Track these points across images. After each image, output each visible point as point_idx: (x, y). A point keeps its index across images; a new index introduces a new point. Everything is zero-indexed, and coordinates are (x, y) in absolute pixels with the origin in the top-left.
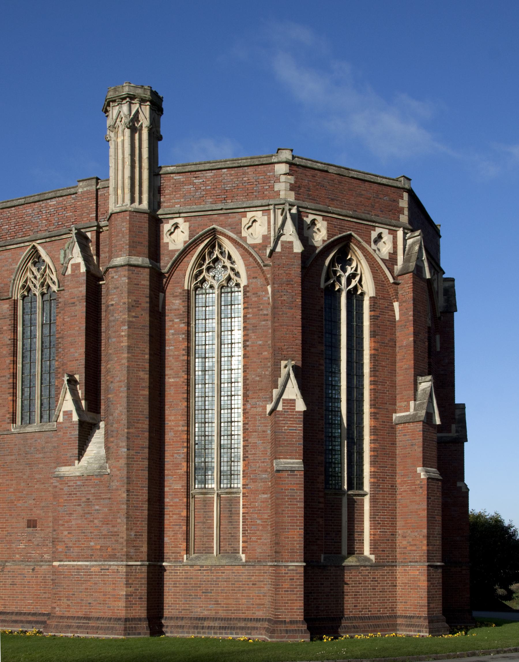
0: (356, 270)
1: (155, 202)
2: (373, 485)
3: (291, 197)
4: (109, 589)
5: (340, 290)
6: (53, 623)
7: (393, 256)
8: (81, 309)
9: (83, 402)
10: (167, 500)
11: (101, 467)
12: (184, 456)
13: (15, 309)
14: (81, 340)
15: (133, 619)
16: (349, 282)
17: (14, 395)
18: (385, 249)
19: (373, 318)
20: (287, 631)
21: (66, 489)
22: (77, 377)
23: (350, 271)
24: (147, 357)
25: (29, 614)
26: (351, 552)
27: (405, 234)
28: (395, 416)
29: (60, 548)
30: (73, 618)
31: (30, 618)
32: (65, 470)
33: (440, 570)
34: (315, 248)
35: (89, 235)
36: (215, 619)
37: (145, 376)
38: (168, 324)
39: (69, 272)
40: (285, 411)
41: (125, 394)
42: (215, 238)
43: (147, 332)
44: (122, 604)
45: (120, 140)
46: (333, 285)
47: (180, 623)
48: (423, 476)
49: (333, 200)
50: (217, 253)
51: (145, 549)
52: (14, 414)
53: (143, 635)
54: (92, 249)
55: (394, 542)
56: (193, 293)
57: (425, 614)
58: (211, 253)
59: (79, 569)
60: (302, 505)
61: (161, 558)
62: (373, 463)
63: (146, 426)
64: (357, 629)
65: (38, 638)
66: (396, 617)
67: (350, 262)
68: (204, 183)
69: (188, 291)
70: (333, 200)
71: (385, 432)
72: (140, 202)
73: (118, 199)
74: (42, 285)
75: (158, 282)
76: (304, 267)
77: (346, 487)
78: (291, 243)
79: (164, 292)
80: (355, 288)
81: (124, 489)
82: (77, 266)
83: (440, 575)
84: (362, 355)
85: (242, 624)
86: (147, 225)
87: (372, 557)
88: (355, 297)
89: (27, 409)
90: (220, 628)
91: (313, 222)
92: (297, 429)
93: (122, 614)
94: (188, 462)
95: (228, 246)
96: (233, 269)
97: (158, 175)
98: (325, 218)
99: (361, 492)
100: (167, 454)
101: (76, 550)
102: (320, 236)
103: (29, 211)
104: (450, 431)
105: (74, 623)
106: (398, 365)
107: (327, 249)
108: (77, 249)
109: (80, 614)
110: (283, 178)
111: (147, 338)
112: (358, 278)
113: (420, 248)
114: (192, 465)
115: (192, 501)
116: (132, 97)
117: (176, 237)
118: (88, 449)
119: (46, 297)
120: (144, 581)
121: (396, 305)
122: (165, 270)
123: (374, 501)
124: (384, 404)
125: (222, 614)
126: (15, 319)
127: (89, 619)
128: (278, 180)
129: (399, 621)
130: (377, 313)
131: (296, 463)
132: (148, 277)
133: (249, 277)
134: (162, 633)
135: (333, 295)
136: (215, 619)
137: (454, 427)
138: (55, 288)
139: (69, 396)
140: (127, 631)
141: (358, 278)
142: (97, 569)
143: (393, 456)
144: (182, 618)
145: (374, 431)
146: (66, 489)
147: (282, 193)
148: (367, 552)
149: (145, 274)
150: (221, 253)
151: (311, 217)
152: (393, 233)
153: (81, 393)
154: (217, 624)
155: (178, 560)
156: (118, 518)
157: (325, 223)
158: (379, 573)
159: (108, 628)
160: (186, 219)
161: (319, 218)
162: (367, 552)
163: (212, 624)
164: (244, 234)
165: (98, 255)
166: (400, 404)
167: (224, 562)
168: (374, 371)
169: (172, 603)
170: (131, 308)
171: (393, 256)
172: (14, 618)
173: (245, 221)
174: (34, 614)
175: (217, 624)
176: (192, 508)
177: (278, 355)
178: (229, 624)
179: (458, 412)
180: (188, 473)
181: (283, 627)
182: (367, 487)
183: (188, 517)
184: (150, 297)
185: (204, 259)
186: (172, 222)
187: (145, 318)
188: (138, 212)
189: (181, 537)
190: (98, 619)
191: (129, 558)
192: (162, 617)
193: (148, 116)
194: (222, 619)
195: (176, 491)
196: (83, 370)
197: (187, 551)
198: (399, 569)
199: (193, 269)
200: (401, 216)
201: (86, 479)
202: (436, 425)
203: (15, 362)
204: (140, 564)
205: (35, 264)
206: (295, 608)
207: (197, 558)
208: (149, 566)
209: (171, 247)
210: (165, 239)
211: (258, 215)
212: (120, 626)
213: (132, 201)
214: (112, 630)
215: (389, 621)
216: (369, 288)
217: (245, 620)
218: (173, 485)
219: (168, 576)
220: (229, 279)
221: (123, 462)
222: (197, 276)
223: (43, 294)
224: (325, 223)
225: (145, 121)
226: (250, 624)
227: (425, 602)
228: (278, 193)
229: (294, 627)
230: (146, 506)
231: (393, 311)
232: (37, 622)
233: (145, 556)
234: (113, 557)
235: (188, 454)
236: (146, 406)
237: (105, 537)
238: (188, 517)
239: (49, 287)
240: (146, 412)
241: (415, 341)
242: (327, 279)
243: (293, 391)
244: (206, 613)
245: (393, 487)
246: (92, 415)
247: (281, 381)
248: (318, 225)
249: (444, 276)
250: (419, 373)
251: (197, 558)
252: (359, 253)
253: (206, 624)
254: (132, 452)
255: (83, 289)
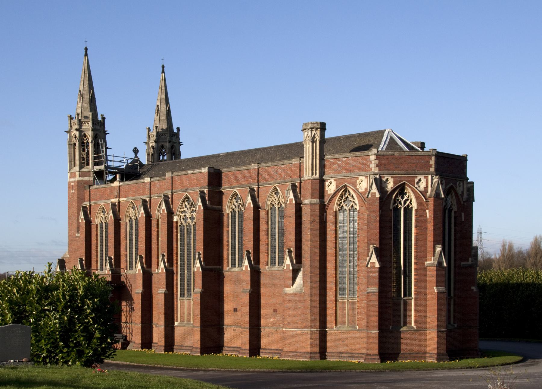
0: (409, 197)
1: (322, 173)
2: (415, 294)
3: (377, 170)
4: (304, 340)
5: (400, 208)
6: (283, 354)
7: (426, 189)
8: (293, 219)
9: (294, 260)
10: (327, 303)
11: (301, 289)
12: (334, 284)
13: (268, 214)
14: (293, 233)
15: (314, 353)
16: (405, 203)
17: (268, 253)
18: (422, 185)
19: (416, 219)
20: (371, 359)
21: (287, 298)
22: (292, 249)
23: (405, 198)
24: (318, 243)
25: (275, 350)
26: (405, 324)
27: (432, 177)
28: (426, 263)
29: (286, 323)
30: (291, 352)
31: (276, 351)
32: (287, 290)
33: (445, 333)
34: (387, 191)
35: (297, 184)
36: (347, 353)
37: (317, 251)
38: (328, 226)
39: (288, 202)
40: (371, 267)
41: (309, 259)
42: (346, 188)
43: (318, 232)
44: (309, 346)
45: (308, 146)
46: (397, 206)
47: (333, 355)
48: (436, 291)
49: (396, 168)
50: (347, 194)
51: (318, 324)
52: (267, 262)
53: (318, 360)
54: (298, 190)
55: (425, 320)
56: (338, 212)
57: (436, 352)
58: (345, 194)
59: (293, 332)
60: (377, 307)
61: (325, 327)
62: (415, 285)
63: (318, 272)
64: (406, 358)
65: (278, 361)
66: (426, 353)
67: (406, 194)
68: (342, 164)
69: (336, 212)
70: (396, 168)
71: (422, 270)
72: (316, 174)
73: (307, 175)
74: (279, 203)
75: (323, 208)
76: (380, 202)
77: (402, 296)
78: (375, 193)
79: (326, 212)
80: (408, 205)
81: (309, 299)
82: (291, 200)
83: (445, 335)
84: (412, 236)
85: (357, 355)
86: (318, 185)
87: (415, 327)
88: (408, 210)
89: (273, 214)
90: (349, 357)
91: (387, 180)
92: (376, 275)
93: (309, 351)
94: (336, 286)
95: (352, 192)
96: (354, 202)
97: (324, 159)
98: (392, 177)
99: (410, 298)
100: (328, 283)
101: (292, 324)
102: (390, 185)
103: (273, 169)
104: (468, 261)
105: (291, 354)
106: (428, 239)
107: (393, 191)
108: (291, 193)
109: (293, 350)
110: (373, 162)
111: (318, 235)
112: (409, 201)
113: (438, 184)
114: (338, 288)
115: (337, 303)
116: (312, 129)
117: (331, 188)
118: (296, 281)
119: (280, 209)
120: (318, 337)
121: (427, 211)
122: (326, 203)
123: (416, 302)
124: (422, 257)
125: (349, 351)
126: (268, 219)
127: (297, 352)
128: (371, 163)
129: (427, 355)
130: (418, 217)
131: (375, 289)
132: (318, 208)
133: (360, 206)
134: (326, 359)
135: (397, 210)
136: (347, 353)
137: (470, 259)
138: (283, 205)
139: (288, 258)
140: (311, 358)
141: (409, 201)
142: (300, 332)
143: (425, 281)
144: (334, 353)
145: (416, 270)
146: (287, 298)
147: (373, 169)
148: (413, 324)
149: (317, 207)
150: (349, 194)
151: (386, 178)
152: (426, 178)
153: (293, 256)
154: (347, 355)
155: (332, 328)
156: (307, 311)
157: (392, 179)
158: (417, 334)
159: (304, 357)
160: (335, 180)
161: (390, 178)
162: (413, 324)
163: (345, 355)
164: (357, 187)
165: (300, 193)
166: (429, 257)
167: (350, 329)
168: (416, 243)
169: (330, 346)
170: (312, 222)
171: (426, 189)
172: (269, 351)
173: (358, 181)
174: (277, 350)
175: (347, 355)
176: (338, 306)
177: (369, 243)
178: (352, 355)
179: (473, 251)
180: (336, 291)
181: (369, 357)
182: (413, 296)
183: (336, 310)
184: (320, 217)
185: (342, 197)
186: (329, 181)
187: (317, 226)
188: (315, 179)
189: (333, 318)
190: (300, 352)
191: (312, 328)
192: (326, 352)
193: (319, 135)
194: (349, 353)
195: (331, 299)
196: (294, 246)
197: (336, 324)
198: (428, 332)
199: (338, 202)
200: (431, 169)
201: (295, 294)
202: (444, 267)
203: (268, 238)
204: (316, 330)
205: (275, 193)
206: (375, 350)
207: (340, 327)
208: (320, 331)
209: (329, 192)
210: (327, 189)
211: (363, 178)
212: (308, 356)
213: (312, 174)
214: (305, 357)
215: (423, 355)
216: (415, 205)
217: (358, 353)
218: (330, 296)
219: (328, 335)
220: (352, 206)
221: (309, 288)
222: (339, 205)
223: (279, 208)
224: (392, 179)
225: (318, 138)
226: (360, 356)
227: (436, 347)
228: (371, 169)
229: (374, 357)
230: (318, 306)
231: (426, 214)
232: (278, 353)
233: (318, 327)
234: (305, 327)
235: (336, 283)
236: (318, 264)
237: (302, 319)
238: (336, 310)
239: (281, 204)
240: (318, 266)
241: (434, 229)
242: (395, 203)
243: (374, 259)
244: (343, 350)
245: (425, 295)
246: (298, 265)
247: (370, 254)
248: (389, 181)
249: (469, 181)
250: (436, 243)
251: (340, 327)
252: (409, 189)
253: (343, 355)
254: (312, 284)
255: (294, 210)
